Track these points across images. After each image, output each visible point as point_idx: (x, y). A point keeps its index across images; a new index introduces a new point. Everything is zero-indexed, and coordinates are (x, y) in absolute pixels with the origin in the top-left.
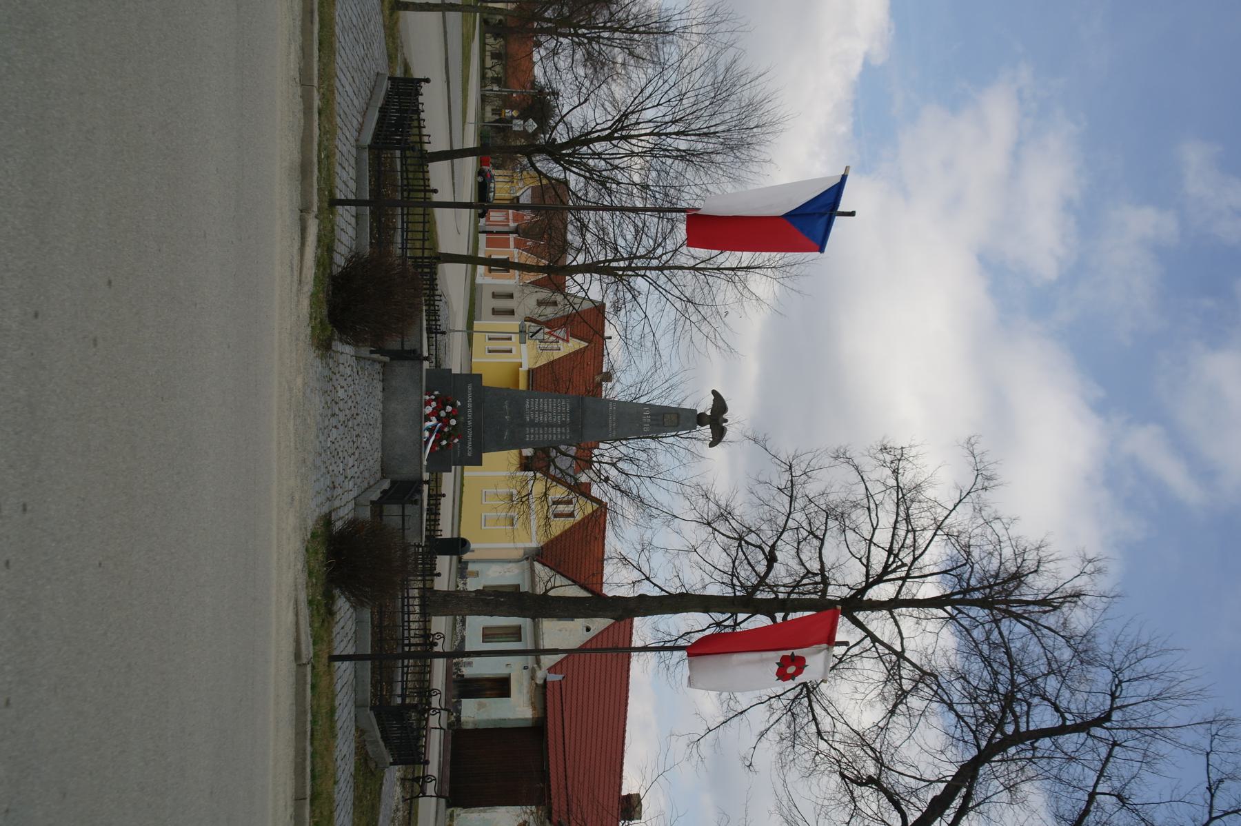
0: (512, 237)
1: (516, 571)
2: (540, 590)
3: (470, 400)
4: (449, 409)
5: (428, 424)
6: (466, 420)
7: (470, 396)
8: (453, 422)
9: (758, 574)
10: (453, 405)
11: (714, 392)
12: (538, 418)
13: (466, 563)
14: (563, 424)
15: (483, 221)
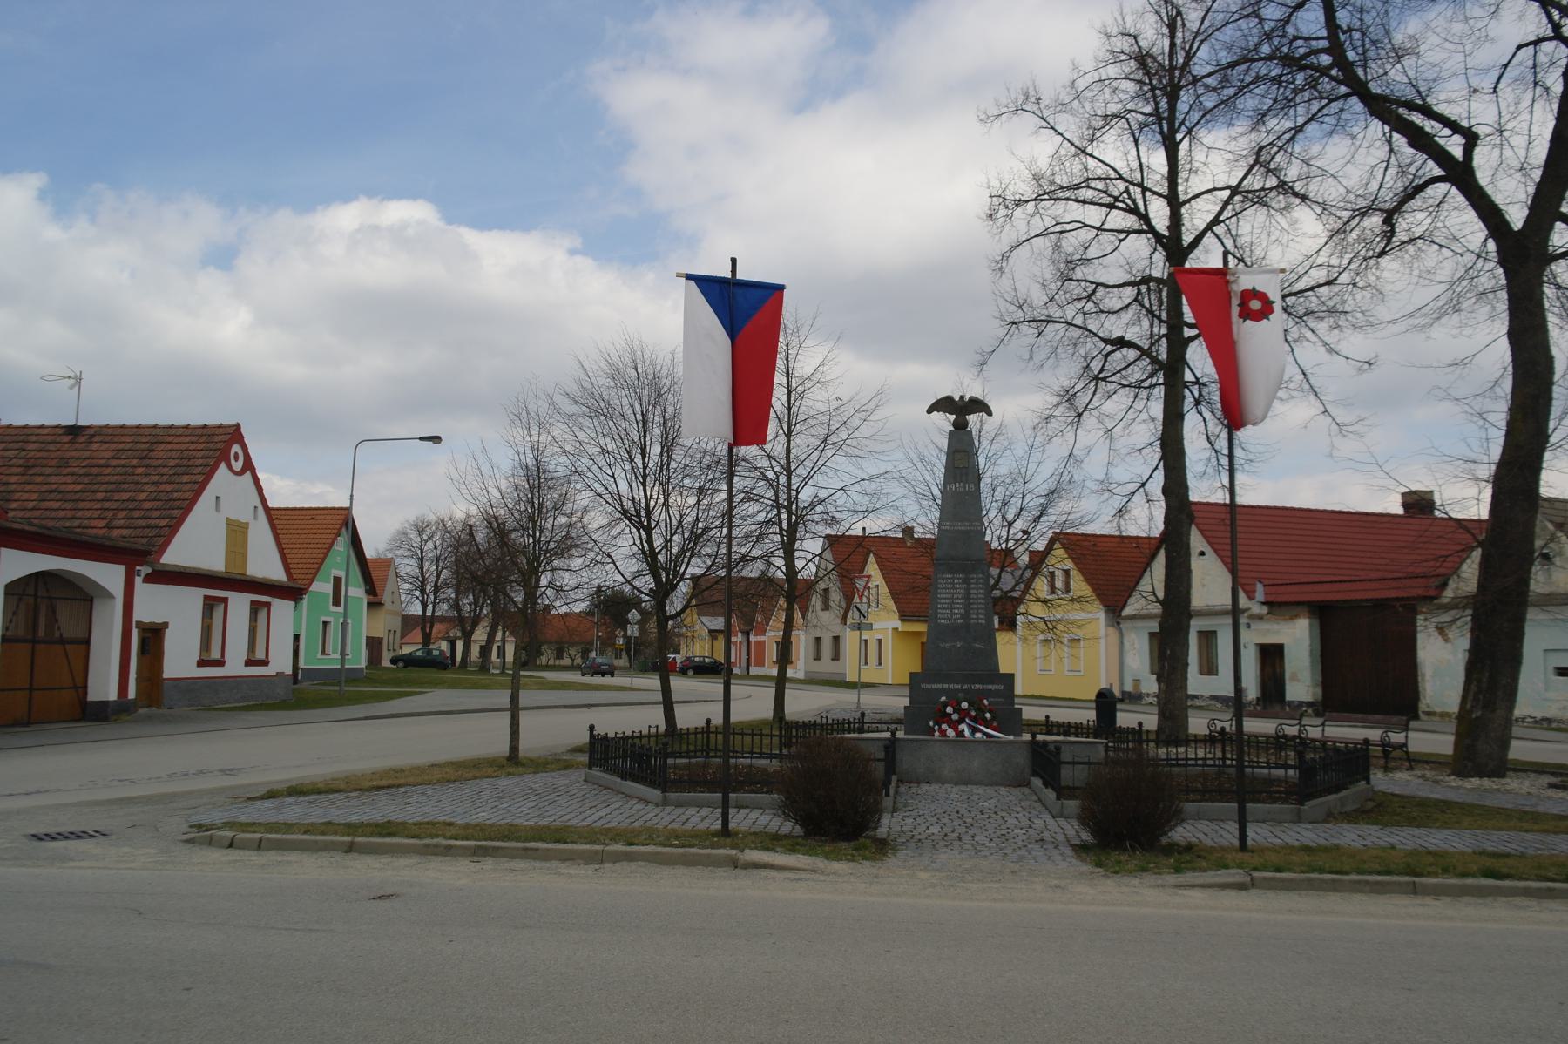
0: (752, 638)
2: (1156, 609)
3: (939, 686)
4: (949, 710)
5: (967, 733)
7: (935, 686)
10: (945, 705)
11: (930, 411)
12: (959, 609)
14: (966, 581)
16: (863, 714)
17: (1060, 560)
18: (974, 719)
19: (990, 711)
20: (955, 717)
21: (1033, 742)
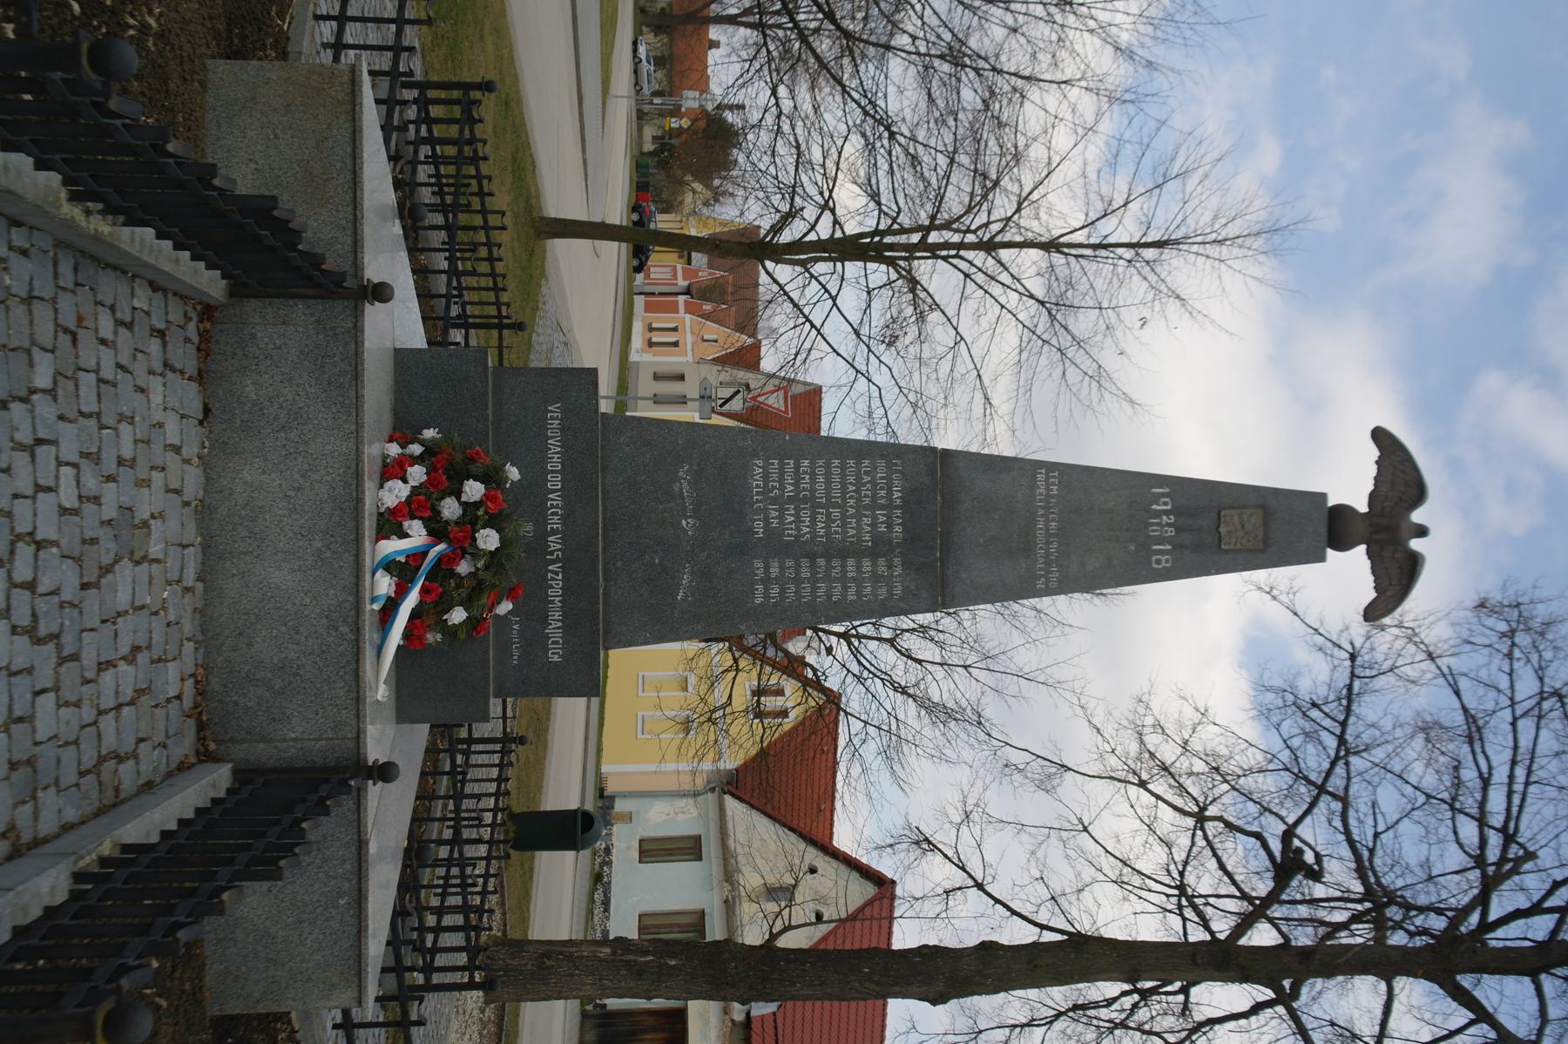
0: (681, 299)
1: (695, 813)
2: (753, 936)
3: (555, 462)
4: (474, 490)
5: (392, 547)
6: (542, 535)
7: (554, 447)
8: (489, 539)
9: (1472, 1023)
10: (491, 478)
11: (1380, 436)
12: (796, 525)
13: (612, 798)
14: (880, 548)
15: (640, 277)
16: (519, 327)
17: (791, 699)
18: (442, 570)
19: (474, 624)
20: (450, 509)
21: (352, 773)
